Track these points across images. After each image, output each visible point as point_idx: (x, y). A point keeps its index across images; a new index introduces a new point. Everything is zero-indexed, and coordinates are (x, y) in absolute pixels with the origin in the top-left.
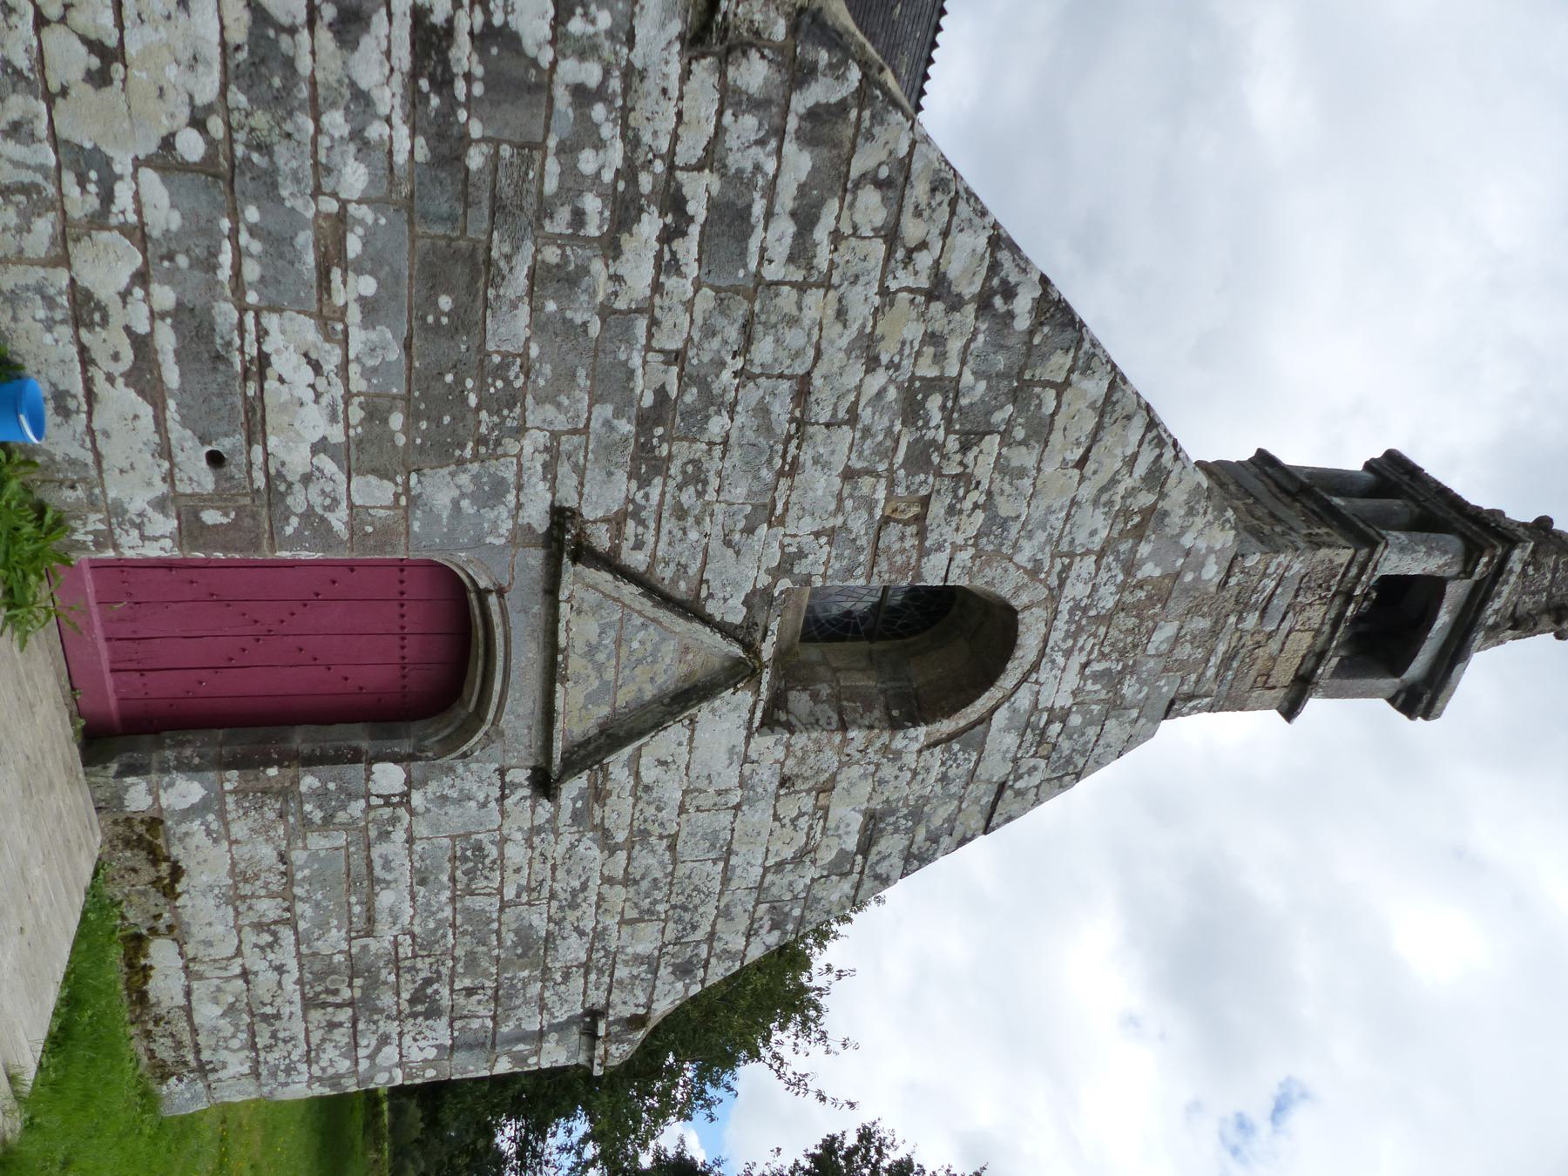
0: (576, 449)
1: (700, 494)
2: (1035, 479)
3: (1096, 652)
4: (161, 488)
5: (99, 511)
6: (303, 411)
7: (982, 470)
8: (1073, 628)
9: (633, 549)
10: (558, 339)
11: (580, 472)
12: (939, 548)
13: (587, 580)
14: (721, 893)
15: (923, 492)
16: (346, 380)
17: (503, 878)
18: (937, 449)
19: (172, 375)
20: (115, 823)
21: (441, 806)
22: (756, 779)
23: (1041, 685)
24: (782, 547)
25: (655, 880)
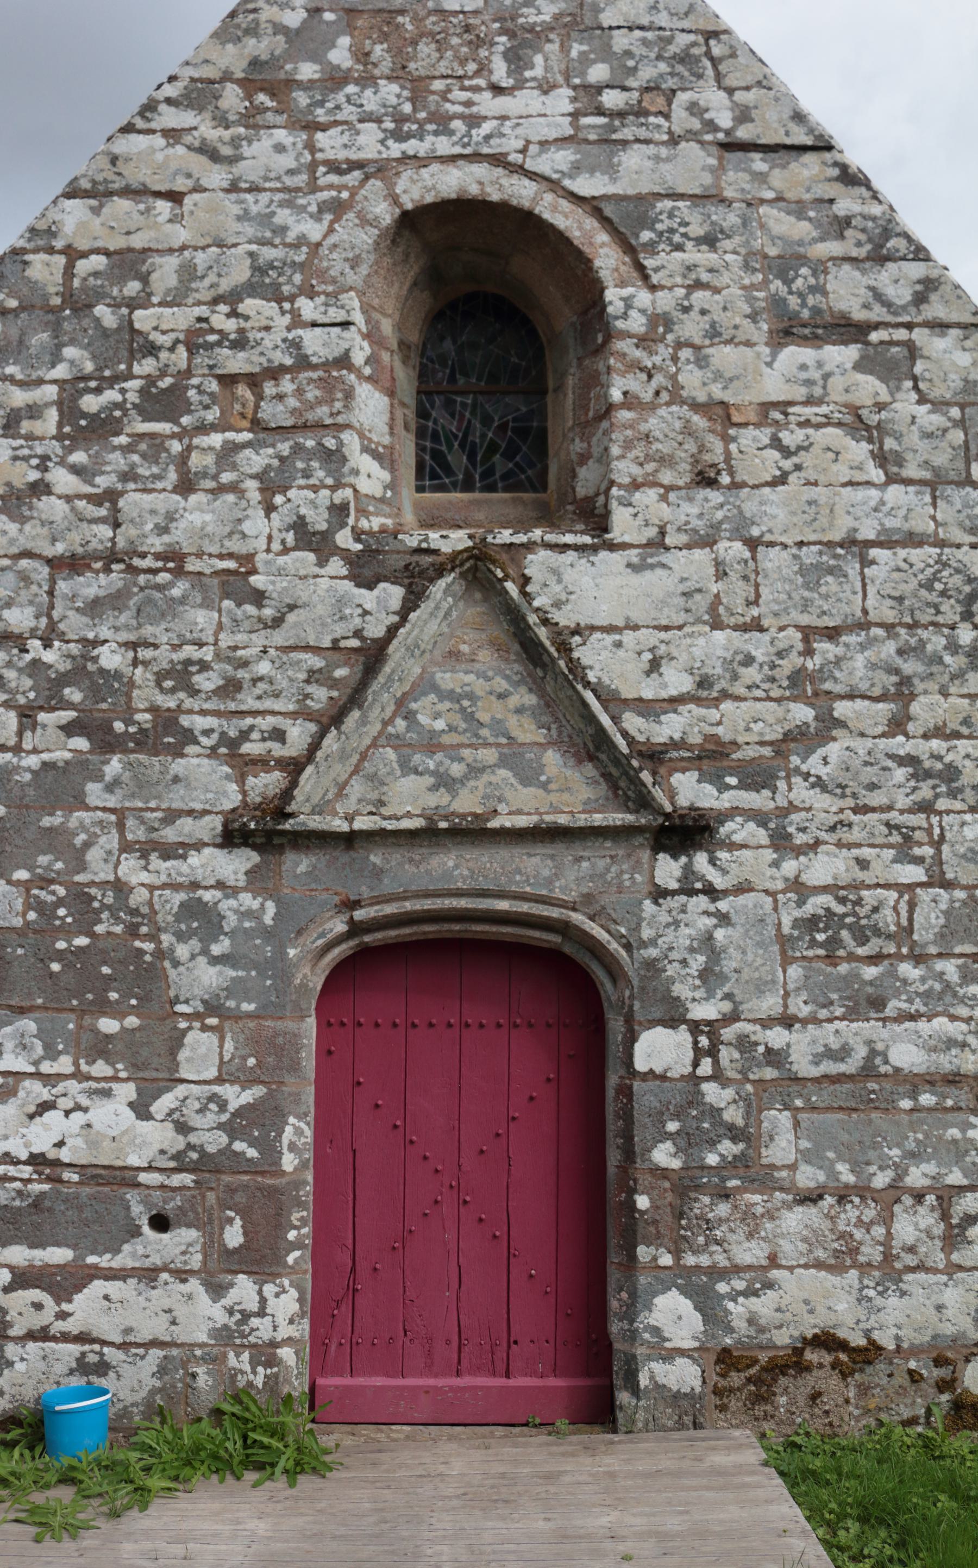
0: (143, 822)
1: (204, 666)
2: (196, 249)
3: (475, 82)
4: (194, 1285)
5: (225, 1355)
6: (97, 1126)
7: (181, 320)
8: (431, 127)
9: (284, 742)
10: (8, 848)
11: (172, 816)
12: (296, 345)
13: (330, 796)
14: (941, 544)
15: (214, 386)
16: (60, 1077)
17: (878, 885)
18: (153, 384)
19: (59, 1255)
20: (723, 1408)
21: (722, 978)
22: (696, 523)
23: (528, 142)
24: (286, 551)
25: (900, 652)
